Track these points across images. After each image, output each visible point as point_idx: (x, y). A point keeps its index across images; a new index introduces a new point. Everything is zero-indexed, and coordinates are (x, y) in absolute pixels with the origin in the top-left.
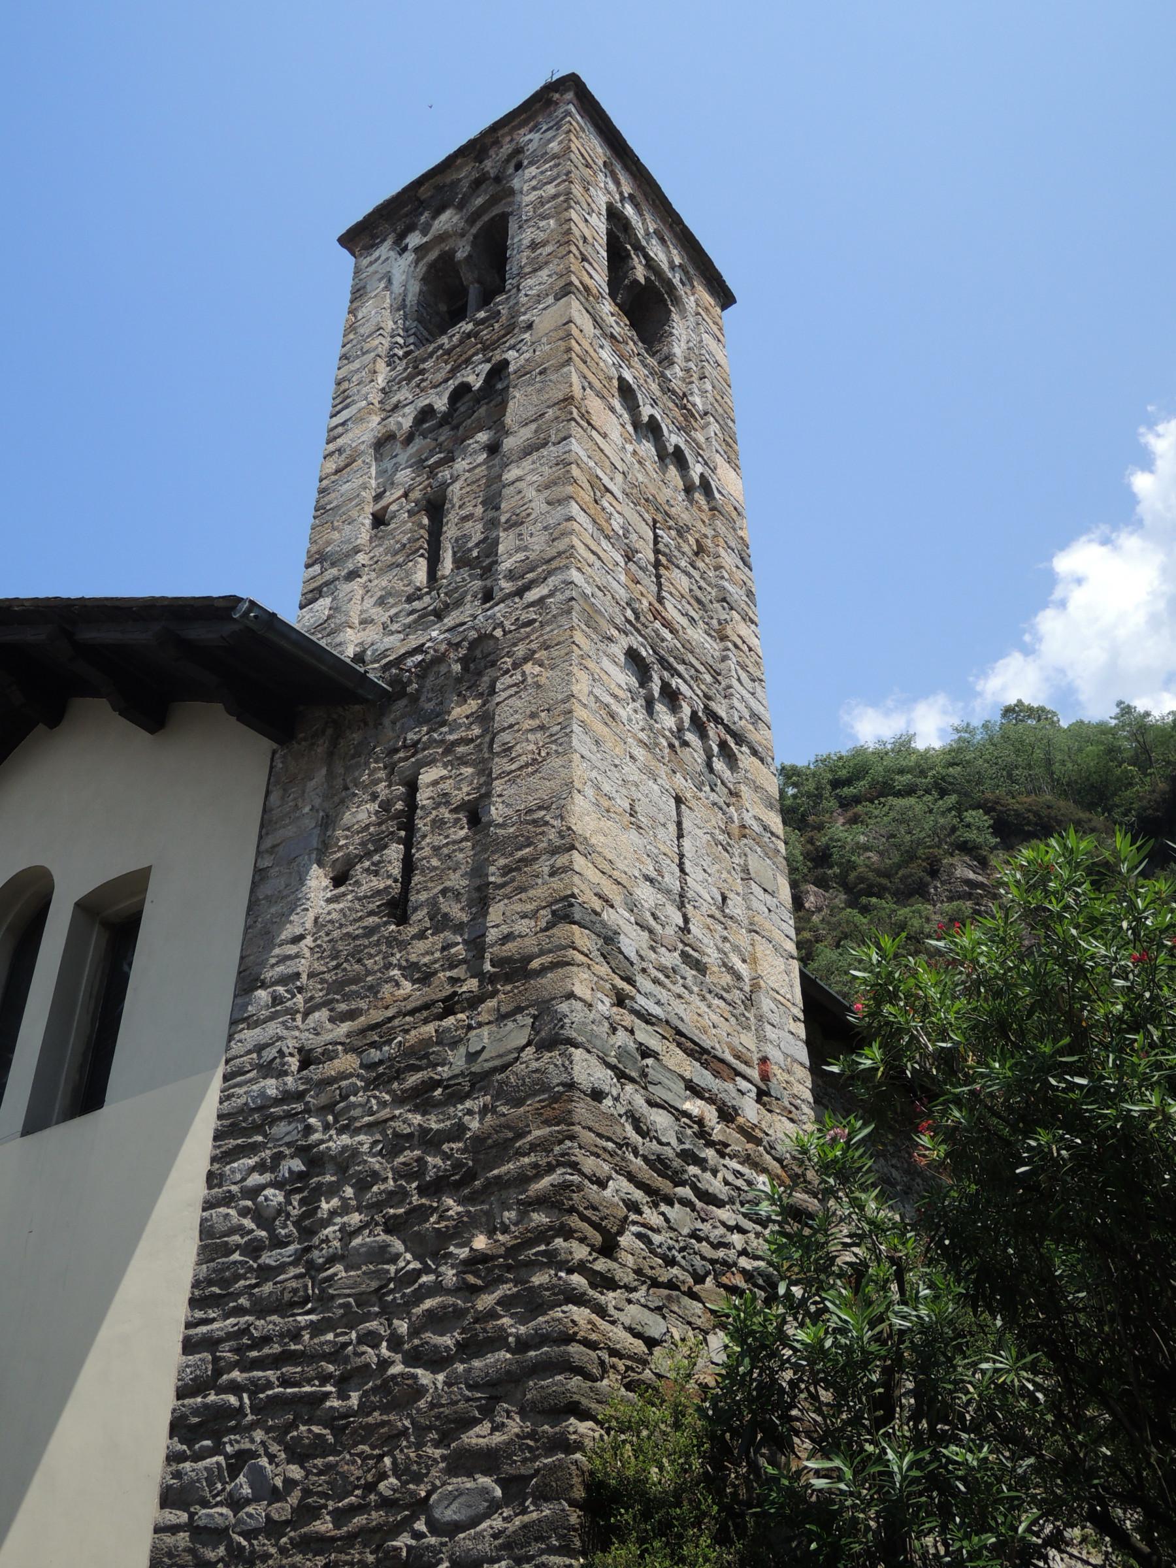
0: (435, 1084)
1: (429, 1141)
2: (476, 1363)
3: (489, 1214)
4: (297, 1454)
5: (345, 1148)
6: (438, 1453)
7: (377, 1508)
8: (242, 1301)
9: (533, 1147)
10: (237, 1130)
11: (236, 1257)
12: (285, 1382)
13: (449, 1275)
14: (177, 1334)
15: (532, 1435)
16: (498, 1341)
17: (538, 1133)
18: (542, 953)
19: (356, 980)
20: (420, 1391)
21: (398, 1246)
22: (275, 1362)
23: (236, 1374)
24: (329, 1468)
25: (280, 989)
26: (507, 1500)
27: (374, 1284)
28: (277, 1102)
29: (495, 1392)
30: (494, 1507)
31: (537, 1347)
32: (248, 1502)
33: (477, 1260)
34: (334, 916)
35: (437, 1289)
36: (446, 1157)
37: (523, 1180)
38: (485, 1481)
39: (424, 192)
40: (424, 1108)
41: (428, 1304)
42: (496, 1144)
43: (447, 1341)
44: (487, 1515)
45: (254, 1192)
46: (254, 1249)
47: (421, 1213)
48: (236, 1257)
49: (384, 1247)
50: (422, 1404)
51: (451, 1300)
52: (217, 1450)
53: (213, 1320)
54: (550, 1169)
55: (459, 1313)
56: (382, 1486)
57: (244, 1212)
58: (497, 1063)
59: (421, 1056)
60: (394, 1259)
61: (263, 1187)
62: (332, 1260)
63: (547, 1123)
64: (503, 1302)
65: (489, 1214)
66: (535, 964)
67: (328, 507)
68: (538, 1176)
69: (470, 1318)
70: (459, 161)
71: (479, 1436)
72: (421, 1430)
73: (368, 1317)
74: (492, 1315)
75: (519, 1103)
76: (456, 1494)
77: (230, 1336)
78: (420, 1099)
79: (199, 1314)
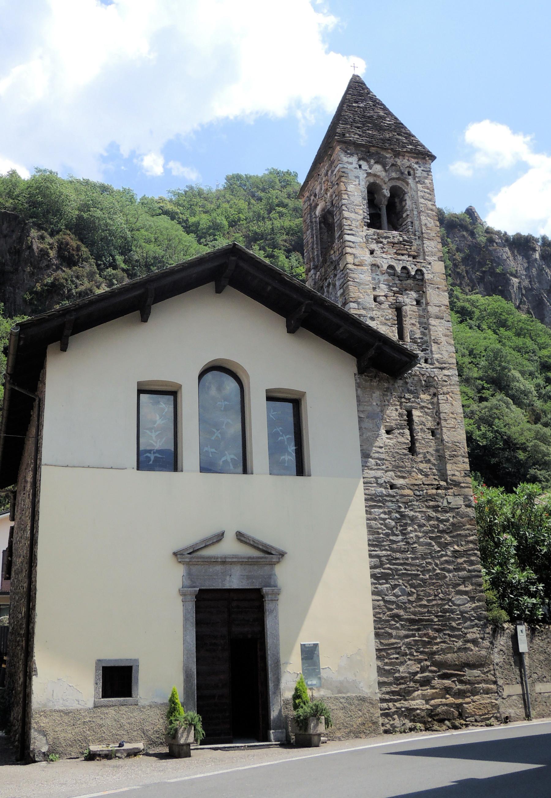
0: (439, 506)
1: (442, 521)
2: (459, 573)
3: (457, 541)
4: (412, 586)
5: (413, 516)
6: (453, 590)
7: (439, 600)
8: (387, 547)
9: (468, 529)
10: (373, 501)
11: (381, 536)
12: (406, 569)
13: (449, 553)
14: (367, 553)
15: (475, 589)
16: (464, 569)
17: (468, 526)
18: (464, 483)
19: (402, 467)
20: (446, 577)
21: (434, 543)
22: (401, 564)
23: (388, 566)
24: (423, 590)
25: (379, 462)
26: (471, 601)
27: (429, 551)
28: (386, 496)
29: (464, 580)
30: (468, 602)
31: (474, 572)
32: (400, 596)
33: (455, 551)
34: (390, 444)
35: (446, 555)
36: (445, 525)
37: (466, 536)
38: (465, 597)
39: (349, 97)
40: (437, 511)
41: (444, 558)
42: (458, 526)
43: (451, 567)
44: (467, 603)
45: (384, 519)
46: (387, 535)
47: (440, 537)
48: (381, 536)
49: (430, 543)
50: (447, 579)
51: (451, 559)
52: (387, 583)
53: (377, 551)
54: (472, 535)
55: (454, 562)
56: (440, 595)
57: (381, 524)
58: (456, 507)
59: (433, 498)
60: (433, 546)
61: (386, 519)
62: (414, 543)
63: (470, 524)
64: (465, 561)
65: (457, 541)
66: (463, 485)
67: (355, 280)
68: (470, 536)
69: (456, 563)
70: (389, 151)
71: (462, 588)
72: (448, 585)
73: (428, 558)
74: (462, 564)
75: (462, 518)
76: (458, 599)
77: (384, 556)
78: (435, 508)
79: (373, 549)
